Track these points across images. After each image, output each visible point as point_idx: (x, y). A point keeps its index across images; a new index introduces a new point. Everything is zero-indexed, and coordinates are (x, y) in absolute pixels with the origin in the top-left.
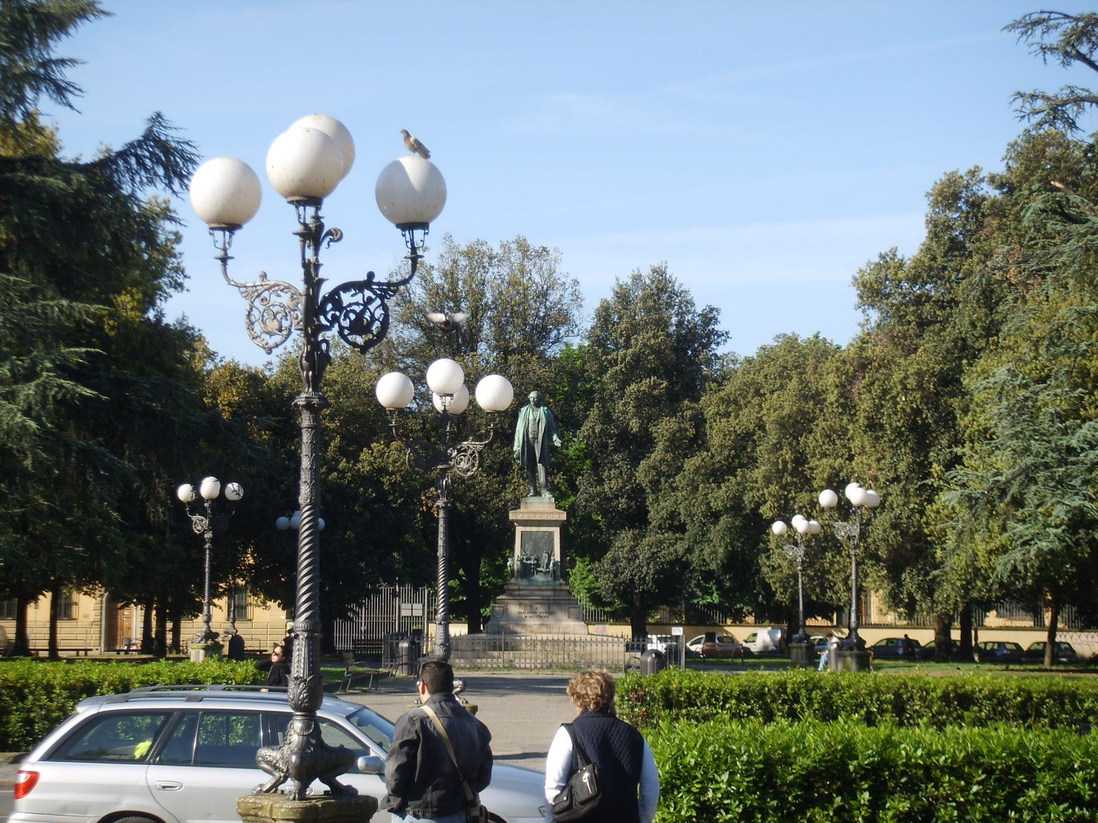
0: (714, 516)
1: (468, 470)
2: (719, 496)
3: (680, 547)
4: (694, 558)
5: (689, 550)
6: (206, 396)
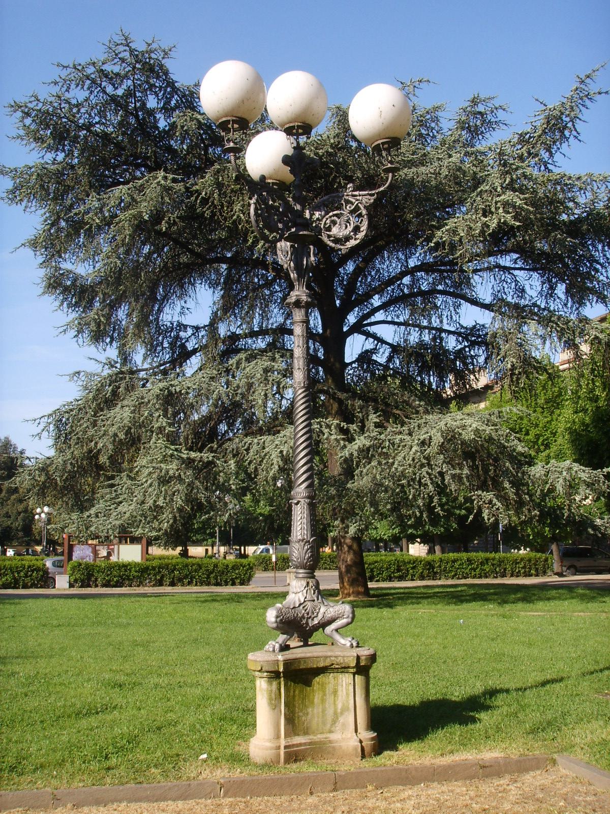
0: (19, 513)
1: (347, 239)
2: (21, 507)
3: (9, 523)
4: (13, 526)
5: (12, 523)
6: (228, 307)
